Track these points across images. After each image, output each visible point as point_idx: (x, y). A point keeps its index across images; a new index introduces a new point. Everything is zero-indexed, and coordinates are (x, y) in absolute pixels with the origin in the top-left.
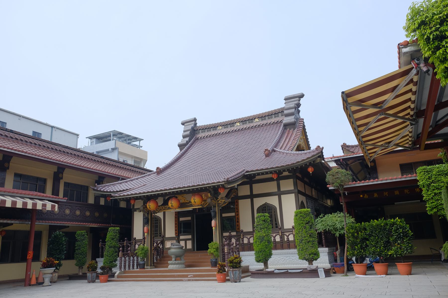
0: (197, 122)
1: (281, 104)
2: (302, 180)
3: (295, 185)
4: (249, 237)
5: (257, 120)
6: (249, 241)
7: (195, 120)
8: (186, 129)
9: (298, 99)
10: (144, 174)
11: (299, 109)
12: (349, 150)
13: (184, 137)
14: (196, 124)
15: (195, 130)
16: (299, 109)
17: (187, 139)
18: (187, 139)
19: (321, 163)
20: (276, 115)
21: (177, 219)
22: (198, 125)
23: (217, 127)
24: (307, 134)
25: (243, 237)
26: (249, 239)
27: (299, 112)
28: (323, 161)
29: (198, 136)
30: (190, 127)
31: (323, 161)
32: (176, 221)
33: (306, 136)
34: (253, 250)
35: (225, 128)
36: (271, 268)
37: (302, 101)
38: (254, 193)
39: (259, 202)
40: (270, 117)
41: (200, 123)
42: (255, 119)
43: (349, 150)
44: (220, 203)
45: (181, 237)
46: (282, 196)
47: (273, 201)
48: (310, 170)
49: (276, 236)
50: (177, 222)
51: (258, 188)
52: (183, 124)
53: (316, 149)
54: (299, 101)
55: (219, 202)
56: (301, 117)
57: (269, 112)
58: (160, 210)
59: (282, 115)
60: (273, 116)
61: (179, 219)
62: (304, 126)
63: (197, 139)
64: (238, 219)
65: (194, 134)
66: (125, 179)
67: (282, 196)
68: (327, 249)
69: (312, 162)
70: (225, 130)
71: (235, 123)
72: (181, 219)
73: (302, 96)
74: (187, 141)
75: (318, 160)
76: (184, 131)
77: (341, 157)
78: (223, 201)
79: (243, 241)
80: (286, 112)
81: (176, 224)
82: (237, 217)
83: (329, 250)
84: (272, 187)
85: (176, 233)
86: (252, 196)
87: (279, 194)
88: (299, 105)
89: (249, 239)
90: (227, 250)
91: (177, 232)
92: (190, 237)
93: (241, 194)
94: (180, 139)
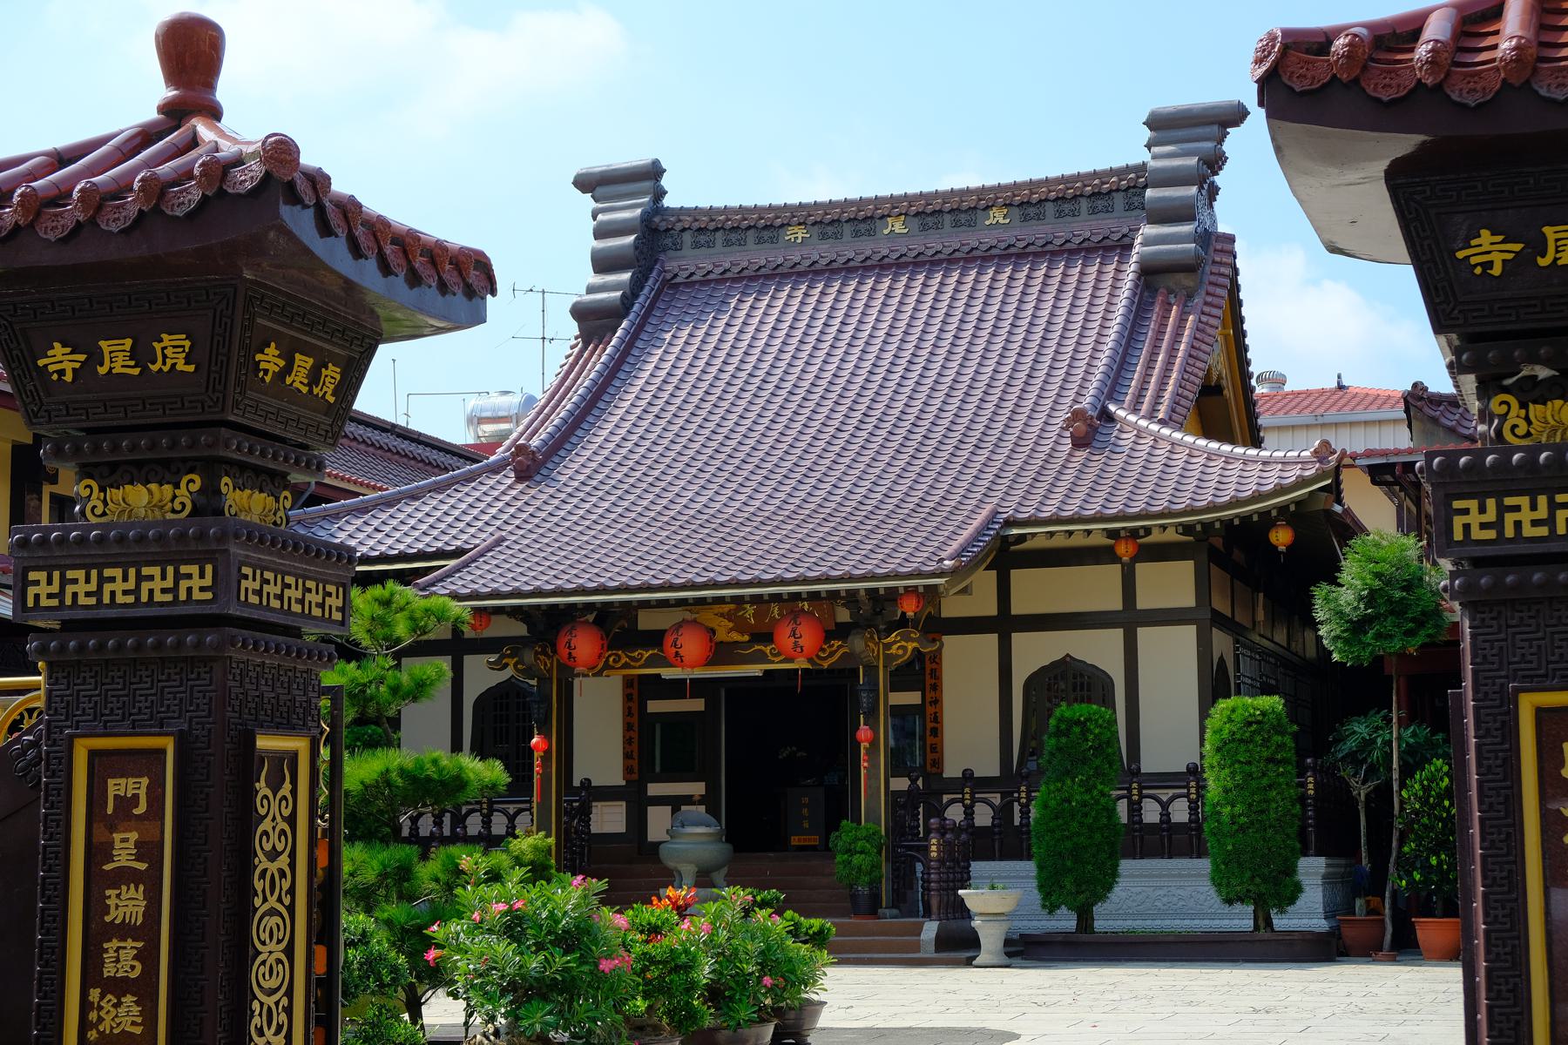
2: (1237, 573)
3: (1203, 586)
4: (1165, 795)
5: (997, 216)
6: (1165, 814)
7: (654, 172)
9: (1215, 128)
10: (446, 470)
11: (1218, 180)
12: (1435, 421)
13: (602, 263)
14: (660, 194)
15: (655, 231)
19: (1329, 513)
20: (1100, 203)
21: (634, 706)
22: (668, 202)
24: (1245, 311)
25: (974, 801)
26: (1165, 806)
27: (1213, 191)
28: (1338, 508)
29: (672, 266)
30: (629, 212)
31: (1338, 508)
32: (628, 712)
33: (1240, 335)
34: (1029, 858)
35: (824, 237)
36: (1106, 919)
38: (1017, 608)
39: (1034, 652)
40: (1067, 207)
43: (1435, 421)
44: (897, 657)
45: (654, 789)
46: (1143, 633)
47: (1100, 650)
48: (1281, 537)
49: (519, 811)
50: (635, 720)
51: (1034, 590)
52: (586, 183)
54: (1221, 141)
55: (894, 650)
56: (1222, 228)
57: (1063, 180)
58: (607, 666)
59: (1130, 207)
60: (1084, 204)
61: (643, 707)
62: (1234, 288)
63: (670, 286)
64: (937, 719)
66: (357, 495)
67: (1143, 633)
68: (1322, 861)
69: (1292, 508)
70: (824, 251)
72: (654, 706)
75: (1323, 502)
76: (600, 233)
77: (1398, 452)
78: (911, 646)
81: (628, 727)
82: (930, 710)
83: (1328, 866)
84: (1097, 588)
85: (628, 770)
86: (1005, 624)
87: (1130, 619)
88: (1215, 162)
89: (1165, 806)
90: (938, 851)
91: (635, 764)
92: (697, 789)
93: (953, 608)
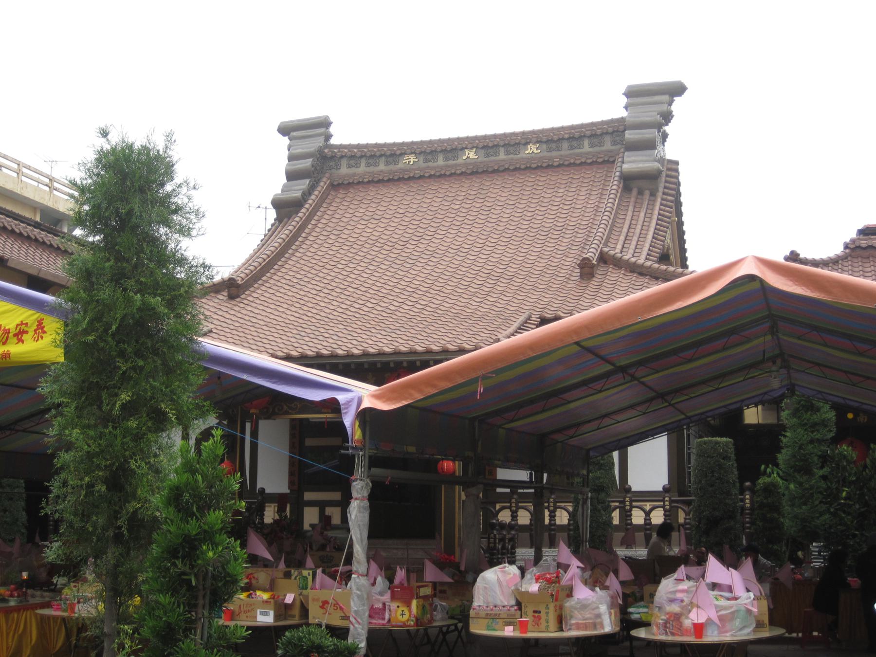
0: (332, 130)
1: (614, 108)
7: (325, 123)
8: (298, 151)
9: (666, 98)
11: (667, 129)
13: (291, 176)
14: (328, 137)
16: (667, 129)
17: (304, 184)
18: (304, 184)
22: (333, 141)
23: (402, 154)
25: (556, 508)
26: (648, 514)
37: (678, 105)
41: (340, 136)
42: (527, 143)
45: (308, 496)
52: (285, 130)
53: (670, 161)
54: (670, 103)
65: (326, 175)
71: (463, 149)
73: (678, 90)
74: (304, 194)
79: (552, 517)
80: (629, 135)
88: (667, 117)
89: (648, 514)
94: (275, 183)
